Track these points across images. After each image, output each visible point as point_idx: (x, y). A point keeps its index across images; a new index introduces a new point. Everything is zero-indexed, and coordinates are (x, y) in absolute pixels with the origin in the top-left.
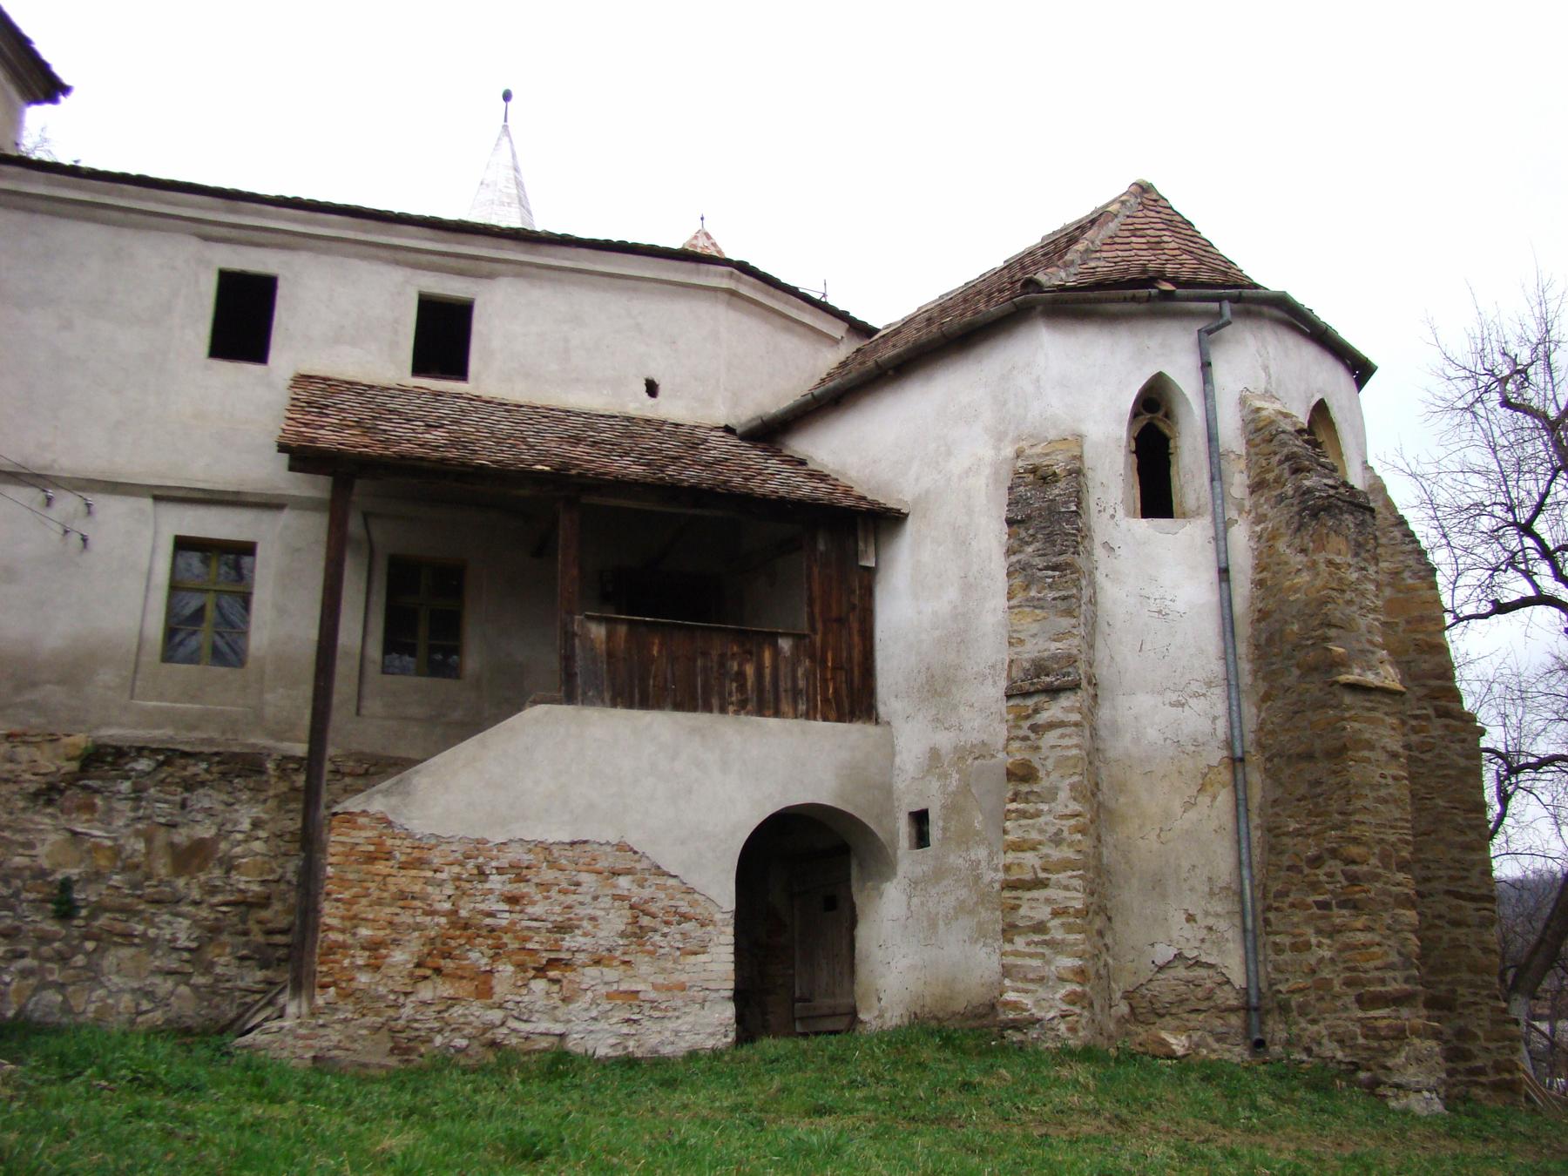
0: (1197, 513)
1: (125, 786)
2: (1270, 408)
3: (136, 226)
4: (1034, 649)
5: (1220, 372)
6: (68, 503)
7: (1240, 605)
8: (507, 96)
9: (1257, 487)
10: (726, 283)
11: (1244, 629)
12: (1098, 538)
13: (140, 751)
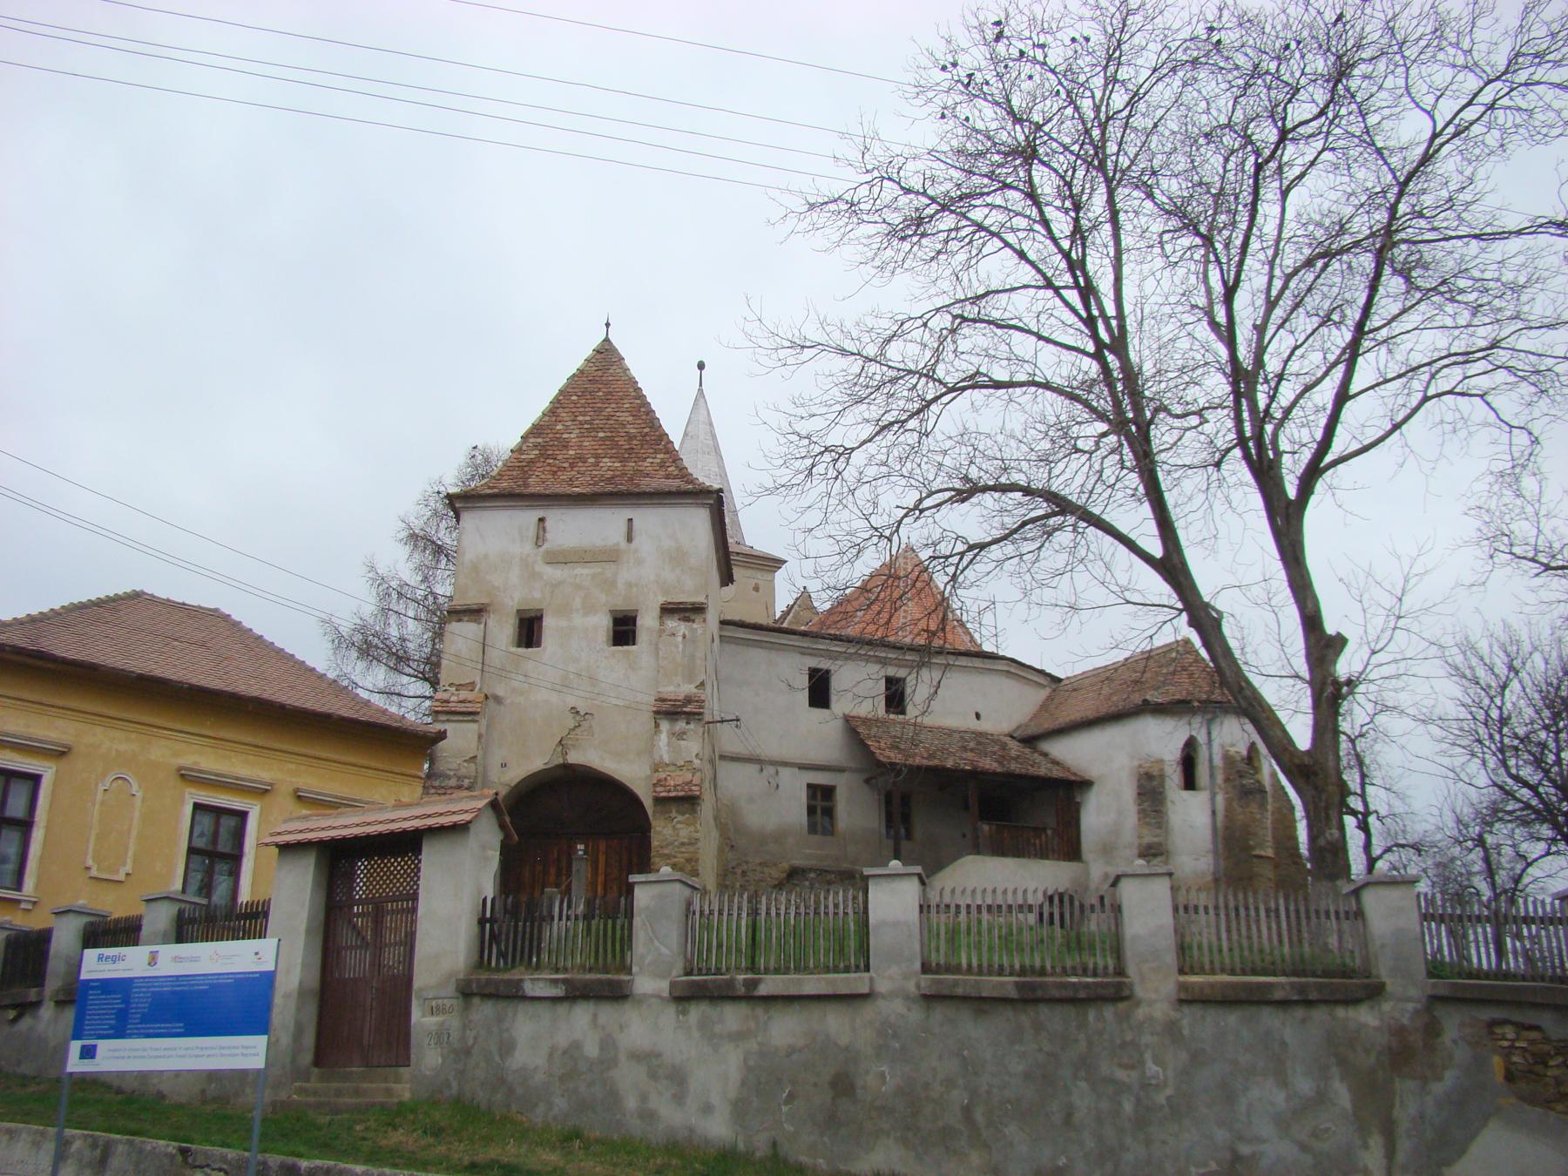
0: (1204, 789)
1: (807, 883)
2: (1232, 750)
3: (777, 650)
4: (1148, 839)
5: (1214, 734)
6: (771, 770)
7: (1219, 824)
8: (701, 366)
9: (1227, 780)
10: (1006, 668)
11: (1220, 833)
12: (1169, 798)
13: (811, 870)
